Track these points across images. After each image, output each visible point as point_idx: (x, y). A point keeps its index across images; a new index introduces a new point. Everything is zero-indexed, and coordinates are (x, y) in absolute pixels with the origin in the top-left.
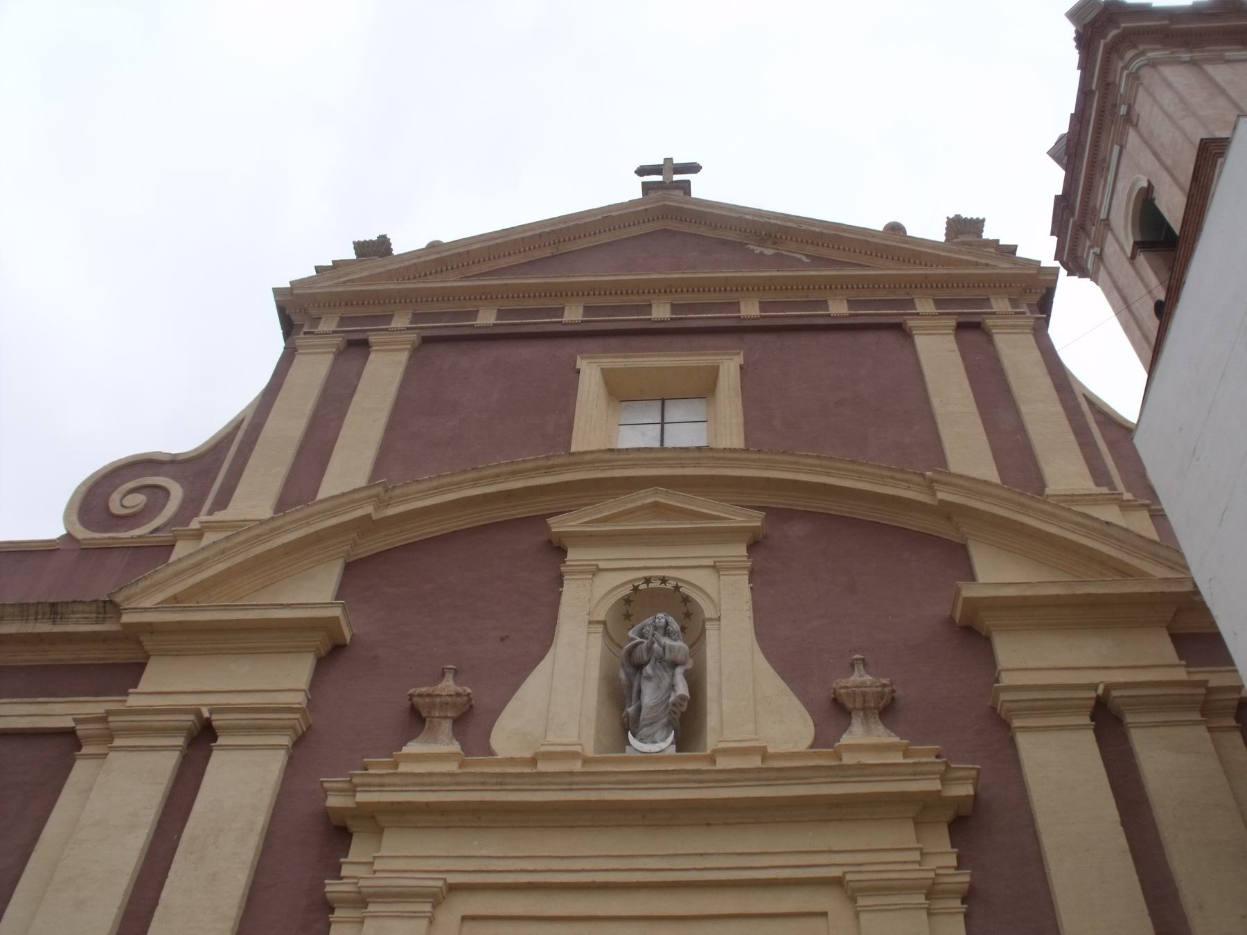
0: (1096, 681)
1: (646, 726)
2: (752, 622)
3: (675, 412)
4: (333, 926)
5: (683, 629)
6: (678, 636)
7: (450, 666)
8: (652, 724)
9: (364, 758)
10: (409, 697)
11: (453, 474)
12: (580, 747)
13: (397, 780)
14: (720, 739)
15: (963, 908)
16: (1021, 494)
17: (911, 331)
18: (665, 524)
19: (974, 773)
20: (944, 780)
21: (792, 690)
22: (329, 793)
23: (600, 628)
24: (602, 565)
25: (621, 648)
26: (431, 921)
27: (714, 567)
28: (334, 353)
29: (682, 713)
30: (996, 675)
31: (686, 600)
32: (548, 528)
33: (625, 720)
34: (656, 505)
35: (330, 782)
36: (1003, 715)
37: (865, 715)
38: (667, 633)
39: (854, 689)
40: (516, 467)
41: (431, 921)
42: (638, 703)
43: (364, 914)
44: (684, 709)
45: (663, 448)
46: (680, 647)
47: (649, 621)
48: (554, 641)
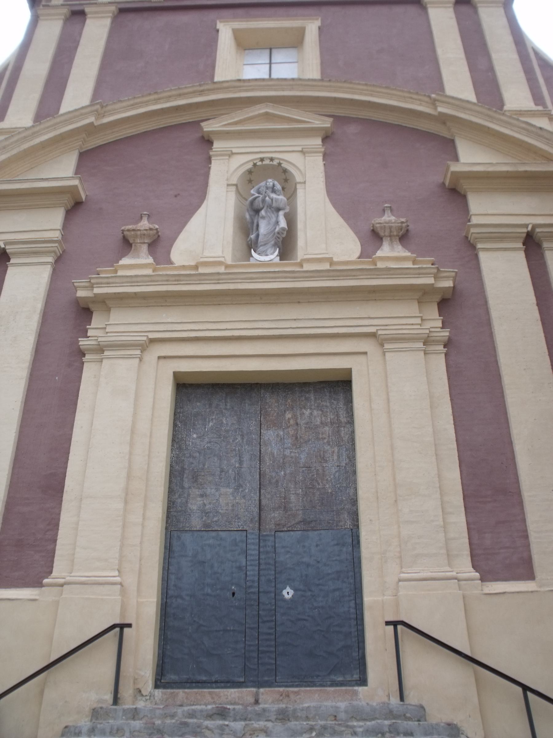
0: (527, 223)
1: (261, 246)
2: (325, 185)
3: (279, 56)
4: (85, 364)
5: (283, 189)
6: (280, 193)
7: (145, 213)
8: (265, 244)
9: (97, 268)
10: (122, 232)
11: (143, 96)
12: (223, 258)
13: (117, 280)
14: (306, 253)
15: (445, 350)
16: (489, 109)
17: (426, 5)
18: (272, 125)
19: (453, 274)
20: (436, 277)
21: (348, 224)
22: (77, 289)
23: (234, 188)
24: (234, 151)
25: (246, 200)
26: (141, 360)
27: (301, 151)
28: (63, 20)
29: (283, 238)
30: (469, 218)
31: (285, 171)
32: (201, 128)
33: (250, 242)
34: (267, 114)
35: (78, 282)
36: (471, 241)
37: (391, 240)
38: (274, 191)
39: (385, 224)
40: (181, 91)
41: (141, 360)
42: (257, 232)
43: (102, 357)
44: (284, 236)
45: (270, 79)
46: (281, 199)
47: (263, 184)
48: (207, 197)
